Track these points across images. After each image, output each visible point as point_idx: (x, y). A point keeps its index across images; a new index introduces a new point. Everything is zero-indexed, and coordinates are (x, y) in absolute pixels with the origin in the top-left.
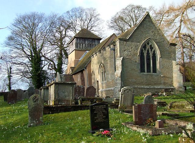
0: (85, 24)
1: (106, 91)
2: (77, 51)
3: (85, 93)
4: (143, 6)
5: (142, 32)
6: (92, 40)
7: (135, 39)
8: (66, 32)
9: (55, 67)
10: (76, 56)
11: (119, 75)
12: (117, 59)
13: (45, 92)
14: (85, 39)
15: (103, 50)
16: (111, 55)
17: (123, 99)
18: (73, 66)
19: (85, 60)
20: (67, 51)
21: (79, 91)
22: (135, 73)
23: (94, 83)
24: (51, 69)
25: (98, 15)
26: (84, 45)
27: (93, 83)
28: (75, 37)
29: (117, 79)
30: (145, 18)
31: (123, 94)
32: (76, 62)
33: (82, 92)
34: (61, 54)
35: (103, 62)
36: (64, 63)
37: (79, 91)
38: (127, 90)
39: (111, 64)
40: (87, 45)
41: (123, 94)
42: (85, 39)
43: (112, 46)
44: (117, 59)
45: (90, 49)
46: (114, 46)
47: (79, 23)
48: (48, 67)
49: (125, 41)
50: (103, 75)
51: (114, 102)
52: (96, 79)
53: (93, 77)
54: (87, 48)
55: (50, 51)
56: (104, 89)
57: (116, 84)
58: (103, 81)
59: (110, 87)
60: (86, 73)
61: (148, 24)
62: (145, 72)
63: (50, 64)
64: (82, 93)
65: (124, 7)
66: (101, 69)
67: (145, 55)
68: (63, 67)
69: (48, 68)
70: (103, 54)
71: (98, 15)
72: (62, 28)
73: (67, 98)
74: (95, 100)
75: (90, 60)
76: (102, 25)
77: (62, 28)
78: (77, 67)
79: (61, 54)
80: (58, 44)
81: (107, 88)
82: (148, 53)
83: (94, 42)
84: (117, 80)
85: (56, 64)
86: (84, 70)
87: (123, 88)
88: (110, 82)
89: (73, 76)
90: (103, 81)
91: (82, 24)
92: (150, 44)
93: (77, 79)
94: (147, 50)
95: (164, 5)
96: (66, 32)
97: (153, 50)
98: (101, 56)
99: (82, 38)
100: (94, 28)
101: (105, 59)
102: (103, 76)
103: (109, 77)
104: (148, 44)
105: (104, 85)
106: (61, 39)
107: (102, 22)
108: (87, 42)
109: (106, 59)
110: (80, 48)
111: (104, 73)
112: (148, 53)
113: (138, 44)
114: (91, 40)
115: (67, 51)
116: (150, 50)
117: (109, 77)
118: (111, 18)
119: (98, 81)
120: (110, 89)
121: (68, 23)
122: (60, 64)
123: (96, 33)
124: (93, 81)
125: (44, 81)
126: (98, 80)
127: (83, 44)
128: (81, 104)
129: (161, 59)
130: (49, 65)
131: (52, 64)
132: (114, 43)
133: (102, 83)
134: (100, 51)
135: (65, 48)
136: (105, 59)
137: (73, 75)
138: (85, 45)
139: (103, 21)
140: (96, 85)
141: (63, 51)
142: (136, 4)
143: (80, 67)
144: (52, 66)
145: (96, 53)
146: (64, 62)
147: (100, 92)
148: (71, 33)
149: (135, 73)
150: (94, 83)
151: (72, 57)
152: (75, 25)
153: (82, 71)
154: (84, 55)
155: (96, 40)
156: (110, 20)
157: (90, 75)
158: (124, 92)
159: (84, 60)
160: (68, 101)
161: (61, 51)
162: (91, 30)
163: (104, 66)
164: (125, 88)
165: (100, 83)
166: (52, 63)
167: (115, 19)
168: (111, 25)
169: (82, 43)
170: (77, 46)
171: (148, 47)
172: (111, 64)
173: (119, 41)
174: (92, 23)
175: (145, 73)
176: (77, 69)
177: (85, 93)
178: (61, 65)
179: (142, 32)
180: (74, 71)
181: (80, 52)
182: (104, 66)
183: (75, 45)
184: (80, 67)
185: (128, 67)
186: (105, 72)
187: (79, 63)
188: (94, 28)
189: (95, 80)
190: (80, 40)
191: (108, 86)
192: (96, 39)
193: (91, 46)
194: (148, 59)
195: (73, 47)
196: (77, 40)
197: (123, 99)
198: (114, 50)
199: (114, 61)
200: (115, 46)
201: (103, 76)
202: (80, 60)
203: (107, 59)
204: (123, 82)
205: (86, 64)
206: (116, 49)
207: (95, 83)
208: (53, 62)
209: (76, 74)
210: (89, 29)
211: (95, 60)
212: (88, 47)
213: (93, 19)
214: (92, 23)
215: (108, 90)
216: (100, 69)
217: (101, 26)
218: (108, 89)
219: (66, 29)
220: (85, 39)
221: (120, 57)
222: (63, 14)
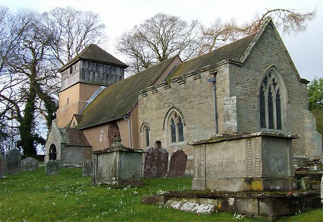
2: (83, 85)
3: (169, 164)
4: (182, 18)
5: (263, 53)
7: (252, 65)
8: (43, 49)
9: (19, 115)
10: (83, 95)
13: (122, 161)
14: (98, 63)
15: (179, 83)
20: (41, 86)
21: (159, 159)
22: (253, 128)
25: (103, 26)
26: (96, 74)
30: (267, 28)
37: (159, 159)
40: (101, 75)
42: (99, 63)
49: (239, 66)
54: (101, 80)
61: (271, 40)
62: (265, 128)
65: (149, 18)
67: (266, 95)
71: (103, 26)
73: (282, 174)
82: (270, 94)
92: (273, 77)
94: (268, 87)
95: (218, 20)
97: (277, 88)
99: (94, 61)
104: (270, 76)
110: (89, 80)
112: (270, 94)
113: (258, 74)
114: (109, 67)
115: (41, 86)
116: (272, 87)
118: (121, 34)
127: (94, 73)
129: (289, 105)
139: (107, 39)
142: (170, 13)
144: (12, 113)
149: (253, 128)
153: (114, 124)
160: (284, 180)
168: (122, 46)
169: (92, 71)
170: (83, 73)
171: (270, 82)
175: (266, 129)
177: (169, 164)
179: (263, 53)
185: (243, 117)
190: (89, 64)
192: (119, 67)
194: (270, 104)
200: (215, 74)
212: (103, 79)
220: (98, 63)
221: (231, 96)
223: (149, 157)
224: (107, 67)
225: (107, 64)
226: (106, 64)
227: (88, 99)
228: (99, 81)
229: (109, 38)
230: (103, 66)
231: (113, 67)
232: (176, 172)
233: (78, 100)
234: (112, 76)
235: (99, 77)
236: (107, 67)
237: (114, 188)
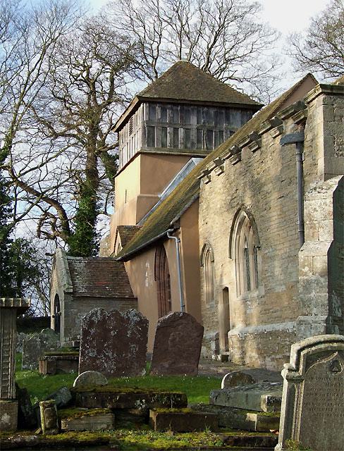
0: (197, 50)
1: (261, 335)
2: (149, 158)
6: (215, 112)
8: (112, 80)
10: (147, 180)
11: (321, 262)
12: (313, 185)
16: (286, 167)
17: (299, 411)
18: (131, 221)
19: (180, 195)
21: (120, 335)
23: (212, 296)
24: (48, 237)
26: (181, 132)
27: (204, 298)
28: (142, 99)
29: (308, 282)
31: (299, 380)
32: (144, 204)
33: (132, 340)
34: (92, 173)
35: (248, 202)
36: (105, 213)
37: (120, 335)
38: (327, 353)
39: (284, 209)
40: (193, 134)
41: (299, 380)
43: (290, 126)
44: (313, 185)
45: (208, 150)
46: (300, 127)
47: (173, 48)
48: (39, 227)
50: (248, 261)
51: (253, 417)
52: (218, 279)
53: (206, 268)
54: (193, 144)
55: (39, 160)
56: (251, 329)
57: (305, 304)
58: (249, 289)
59: (281, 319)
60: (175, 249)
63: (46, 213)
64: (134, 347)
66: (242, 233)
68: (98, 226)
69: (39, 231)
70: (249, 166)
72: (96, 66)
74: (140, 405)
75: (196, 196)
76: (269, 52)
77: (96, 66)
78: (147, 224)
79: (92, 173)
80: (79, 131)
81: (265, 323)
83: (228, 119)
84: (308, 285)
85: (71, 212)
86: (165, 239)
87: (303, 343)
88: (278, 296)
89: (128, 265)
90: (249, 289)
91: (186, 50)
93: (141, 275)
96: (112, 80)
98: (244, 173)
99: (173, 103)
100: (235, 68)
101: (257, 187)
102: (248, 267)
103: (277, 271)
105: (254, 310)
106: (92, 114)
107: (272, 38)
108: (193, 121)
109: (265, 188)
110: (164, 145)
111: (255, 253)
114: (212, 111)
117: (277, 271)
118: (308, 24)
119: (226, 289)
120: (279, 327)
121: (124, 46)
122: (89, 215)
123: (246, 89)
124: (206, 288)
125: (19, 284)
126: (226, 283)
127: (176, 130)
128: (54, 426)
130: (42, 220)
131: (53, 217)
132: (303, 106)
133: (245, 301)
134: (237, 152)
135: (111, 148)
136: (257, 187)
137: (125, 259)
138: (187, 131)
140: (220, 307)
141: (99, 161)
143: (157, 225)
144: (54, 226)
145: (219, 163)
146: (102, 209)
147: (235, 339)
148: (133, 85)
150: (212, 296)
151: (129, 183)
152: (155, 54)
153: (158, 245)
154: (182, 173)
155: (234, 113)
156: (305, 34)
157: (196, 260)
158: (307, 365)
159: (177, 193)
161: (92, 160)
162: (226, 74)
163: (252, 221)
164: (312, 340)
165: (234, 299)
166: (53, 211)
167: (328, 27)
169: (170, 124)
170: (149, 136)
172: (284, 209)
173: (322, 97)
174: (228, 45)
176: (145, 237)
178: (93, 221)
180: (130, 244)
181: (164, 164)
182: (252, 221)
183: (144, 133)
184: (157, 227)
186: (257, 248)
187: (158, 210)
188: (237, 69)
189: (215, 285)
190: (164, 111)
191: (268, 314)
193: (211, 135)
195: (133, 142)
196: (151, 111)
197: (299, 411)
198: (300, 144)
199: (297, 196)
200: (303, 122)
201: (248, 267)
202: (161, 195)
203: (268, 187)
204: (340, 295)
205: (175, 210)
206: (308, 137)
207: (213, 299)
208: (60, 207)
209: (131, 257)
210: (214, 66)
211: (215, 192)
212: (199, 141)
213: (232, 28)
214: (228, 45)
215: (270, 333)
216: (234, 236)
217: (264, 57)
218: (269, 328)
219: (115, 70)
221: (328, 176)
222: (103, 9)
223: (92, 331)
224: (207, 113)
225: (208, 106)
226: (204, 106)
227: (160, 190)
228: (189, 145)
229: (277, 33)
230: (198, 112)
231: (224, 111)
232: (170, 365)
233: (139, 193)
234: (221, 132)
235: (187, 137)
236: (207, 113)
237: (122, 409)
